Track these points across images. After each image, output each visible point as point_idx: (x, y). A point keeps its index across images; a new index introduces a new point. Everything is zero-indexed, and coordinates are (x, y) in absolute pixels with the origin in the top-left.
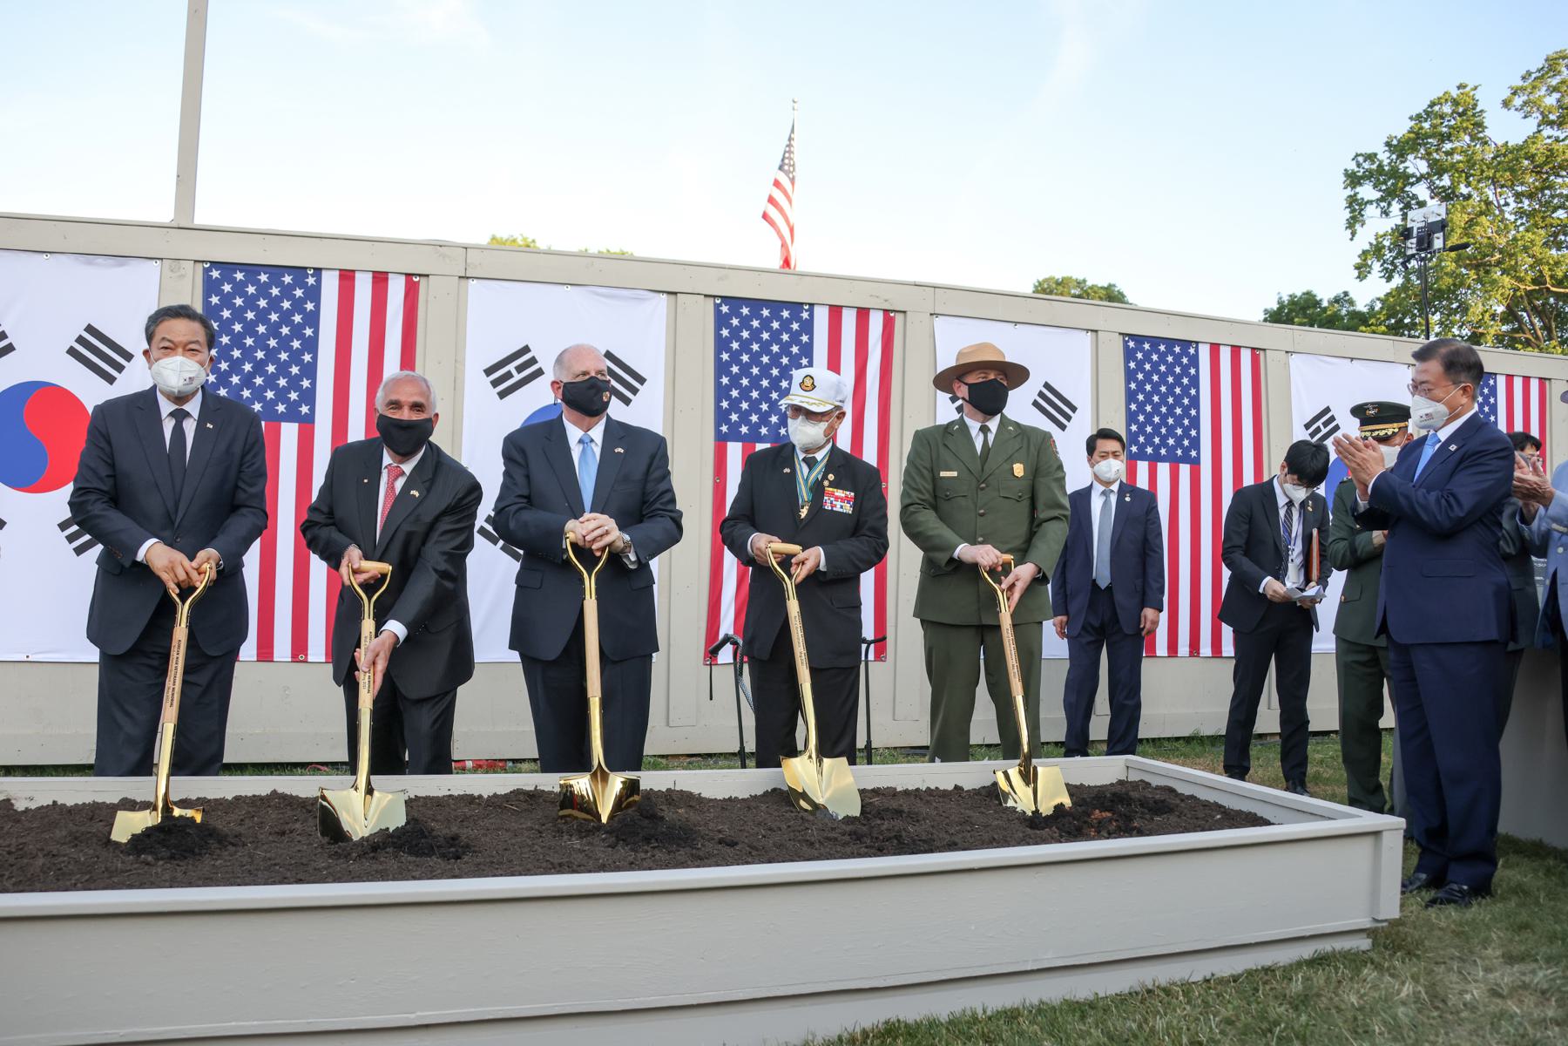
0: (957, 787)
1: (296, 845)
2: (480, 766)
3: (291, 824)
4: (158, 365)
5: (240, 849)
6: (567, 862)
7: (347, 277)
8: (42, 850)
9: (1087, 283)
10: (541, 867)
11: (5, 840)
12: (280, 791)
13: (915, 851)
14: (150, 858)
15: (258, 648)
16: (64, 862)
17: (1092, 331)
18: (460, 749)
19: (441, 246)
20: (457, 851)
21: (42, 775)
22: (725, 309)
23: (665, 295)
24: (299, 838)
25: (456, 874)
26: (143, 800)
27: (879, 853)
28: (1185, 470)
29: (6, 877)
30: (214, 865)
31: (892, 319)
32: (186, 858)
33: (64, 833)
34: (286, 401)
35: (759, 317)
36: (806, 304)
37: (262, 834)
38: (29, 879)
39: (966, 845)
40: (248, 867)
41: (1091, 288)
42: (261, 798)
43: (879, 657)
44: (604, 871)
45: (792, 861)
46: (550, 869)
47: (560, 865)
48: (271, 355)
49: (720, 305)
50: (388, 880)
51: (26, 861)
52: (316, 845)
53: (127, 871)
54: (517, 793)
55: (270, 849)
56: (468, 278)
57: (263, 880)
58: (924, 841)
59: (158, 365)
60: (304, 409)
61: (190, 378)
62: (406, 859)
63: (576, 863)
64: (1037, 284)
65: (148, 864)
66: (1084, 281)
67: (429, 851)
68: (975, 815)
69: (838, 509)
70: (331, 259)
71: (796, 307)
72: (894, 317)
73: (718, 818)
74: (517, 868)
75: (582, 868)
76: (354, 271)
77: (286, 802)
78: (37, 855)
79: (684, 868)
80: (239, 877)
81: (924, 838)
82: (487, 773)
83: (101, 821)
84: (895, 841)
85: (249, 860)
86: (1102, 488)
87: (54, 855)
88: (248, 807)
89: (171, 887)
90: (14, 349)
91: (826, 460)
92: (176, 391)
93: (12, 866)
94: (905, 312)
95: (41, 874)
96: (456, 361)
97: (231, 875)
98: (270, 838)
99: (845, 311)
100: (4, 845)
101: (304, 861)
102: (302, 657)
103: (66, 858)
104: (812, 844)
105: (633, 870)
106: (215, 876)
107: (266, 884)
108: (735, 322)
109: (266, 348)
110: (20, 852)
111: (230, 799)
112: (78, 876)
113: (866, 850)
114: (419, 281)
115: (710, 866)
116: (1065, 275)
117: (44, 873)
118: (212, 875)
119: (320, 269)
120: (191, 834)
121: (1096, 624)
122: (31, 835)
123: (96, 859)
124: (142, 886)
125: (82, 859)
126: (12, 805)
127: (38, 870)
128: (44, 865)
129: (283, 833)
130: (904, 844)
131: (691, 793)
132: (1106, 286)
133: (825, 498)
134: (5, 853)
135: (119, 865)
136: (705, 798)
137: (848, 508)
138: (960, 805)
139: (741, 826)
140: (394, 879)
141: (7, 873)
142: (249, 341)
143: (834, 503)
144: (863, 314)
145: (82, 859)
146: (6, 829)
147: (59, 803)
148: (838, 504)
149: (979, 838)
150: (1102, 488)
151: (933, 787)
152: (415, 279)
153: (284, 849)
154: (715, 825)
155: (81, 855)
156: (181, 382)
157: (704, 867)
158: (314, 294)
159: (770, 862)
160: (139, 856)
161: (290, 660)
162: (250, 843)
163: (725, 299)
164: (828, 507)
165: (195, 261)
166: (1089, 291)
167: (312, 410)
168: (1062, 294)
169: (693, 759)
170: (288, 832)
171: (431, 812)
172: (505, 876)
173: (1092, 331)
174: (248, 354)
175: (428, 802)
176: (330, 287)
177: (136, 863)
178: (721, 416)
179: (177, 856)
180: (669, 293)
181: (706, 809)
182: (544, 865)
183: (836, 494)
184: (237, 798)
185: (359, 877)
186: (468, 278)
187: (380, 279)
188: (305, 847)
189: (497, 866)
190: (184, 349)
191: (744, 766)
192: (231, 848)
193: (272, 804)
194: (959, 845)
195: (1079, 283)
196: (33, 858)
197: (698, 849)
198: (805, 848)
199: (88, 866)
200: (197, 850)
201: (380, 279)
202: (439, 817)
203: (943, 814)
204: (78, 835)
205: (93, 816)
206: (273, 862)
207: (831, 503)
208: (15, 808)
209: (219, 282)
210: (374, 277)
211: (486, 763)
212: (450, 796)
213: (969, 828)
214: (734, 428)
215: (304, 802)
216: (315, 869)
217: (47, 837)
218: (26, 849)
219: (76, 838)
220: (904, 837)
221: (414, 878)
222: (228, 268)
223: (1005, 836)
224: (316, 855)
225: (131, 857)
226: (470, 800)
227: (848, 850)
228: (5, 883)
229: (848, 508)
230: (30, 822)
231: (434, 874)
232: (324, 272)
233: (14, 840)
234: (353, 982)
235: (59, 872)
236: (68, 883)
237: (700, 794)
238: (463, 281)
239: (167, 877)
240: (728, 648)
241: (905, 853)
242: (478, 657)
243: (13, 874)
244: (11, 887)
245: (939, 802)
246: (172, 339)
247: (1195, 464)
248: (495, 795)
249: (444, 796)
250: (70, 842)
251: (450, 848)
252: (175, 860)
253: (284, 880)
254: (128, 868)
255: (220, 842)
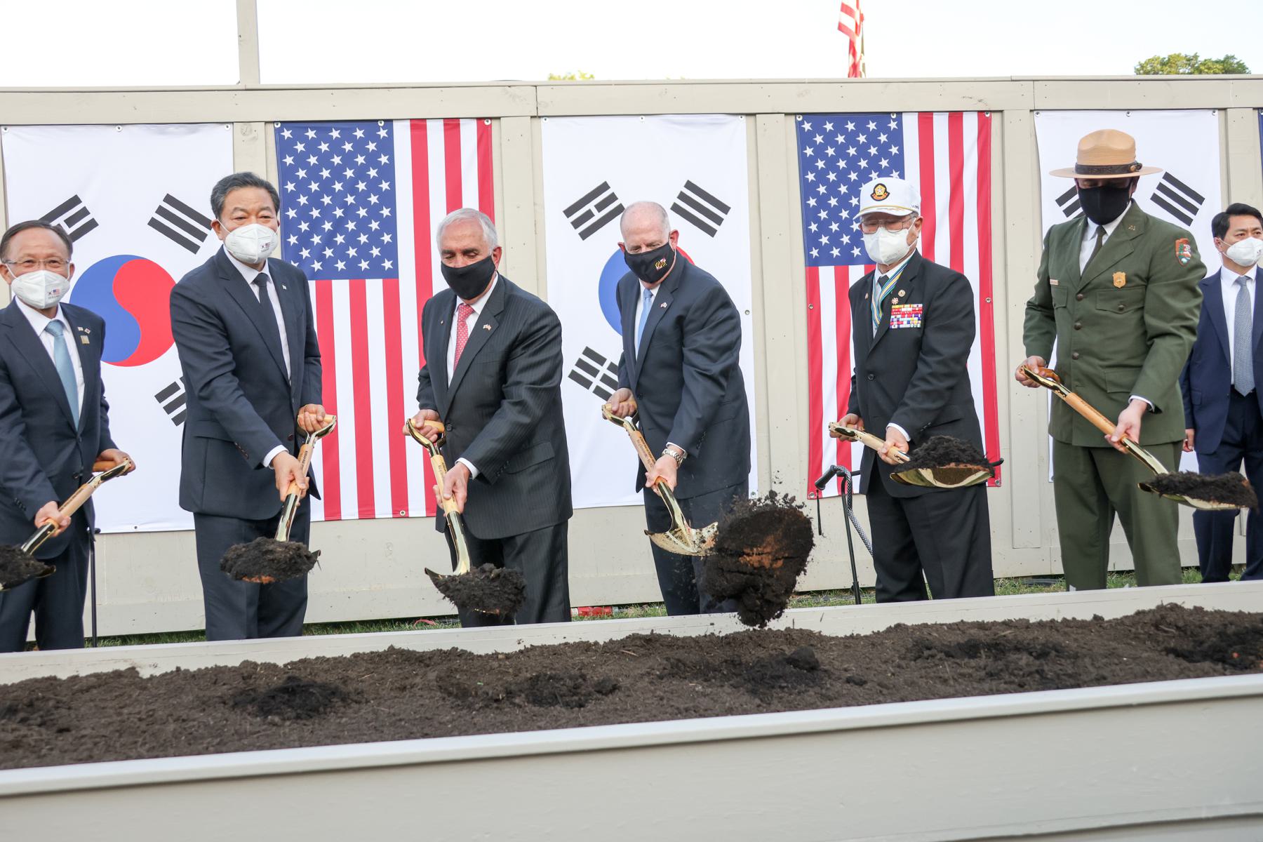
0: (1096, 618)
1: (418, 700)
2: (586, 613)
3: (411, 679)
4: (234, 235)
5: (363, 706)
6: (694, 707)
7: (418, 126)
8: (171, 715)
9: (1199, 59)
10: (666, 713)
11: (135, 707)
12: (397, 646)
13: (1060, 686)
14: (277, 719)
15: (359, 507)
16: (194, 726)
17: (1219, 109)
18: (579, 595)
19: (509, 87)
20: (580, 699)
21: (157, 642)
22: (807, 126)
23: (744, 117)
24: (421, 693)
25: (583, 722)
26: (268, 662)
27: (1021, 689)
28: (374, 288)
29: (139, 744)
30: (340, 723)
31: (989, 120)
32: (311, 717)
33: (191, 698)
34: (368, 257)
35: (866, 131)
36: (893, 113)
37: (383, 690)
38: (162, 745)
39: (1117, 679)
40: (373, 723)
41: (1203, 64)
42: (379, 655)
43: (994, 483)
44: (732, 715)
45: (927, 699)
46: (676, 714)
47: (687, 710)
48: (350, 212)
49: (802, 123)
50: (514, 731)
51: (157, 727)
52: (438, 698)
53: (255, 733)
54: (634, 639)
55: (393, 705)
56: (540, 117)
57: (390, 737)
58: (1070, 676)
59: (234, 235)
60: (387, 265)
61: (266, 244)
62: (530, 709)
63: (702, 707)
64: (1138, 67)
65: (275, 725)
66: (1196, 57)
67: (553, 700)
68: (1121, 648)
69: (905, 325)
70: (401, 109)
71: (882, 117)
72: (491, 125)
73: (842, 655)
74: (642, 714)
75: (709, 712)
76: (425, 120)
77: (404, 657)
78: (168, 720)
79: (813, 709)
80: (366, 734)
81: (1070, 672)
82: (594, 619)
83: (224, 684)
84: (1037, 676)
85: (374, 717)
86: (1236, 276)
87: (184, 720)
88: (367, 663)
89: (301, 746)
90: (97, 225)
91: (897, 277)
92: (256, 258)
93: (144, 732)
94: (1001, 111)
95: (174, 739)
96: (535, 204)
97: (358, 733)
98: (392, 694)
99: (936, 117)
100: (134, 712)
101: (428, 715)
102: (403, 513)
103: (195, 723)
104: (945, 681)
105: (761, 712)
106: (342, 734)
107: (393, 739)
108: (819, 139)
109: (344, 205)
110: (151, 719)
111: (348, 656)
112: (209, 740)
113: (1006, 686)
114: (491, 124)
115: (840, 706)
116: (1172, 53)
117: (176, 738)
118: (339, 734)
119: (391, 121)
120: (314, 694)
121: (1237, 437)
122: (159, 700)
123: (225, 722)
124: (271, 747)
125: (212, 723)
126: (138, 673)
127: (170, 736)
128: (175, 730)
129: (404, 688)
130: (1048, 679)
131: (811, 632)
132: (1222, 59)
133: (892, 317)
134: (136, 720)
135: (248, 727)
136: (825, 636)
137: (916, 322)
138: (1101, 636)
139: (868, 664)
140: (520, 730)
141: (140, 740)
142: (327, 200)
143: (901, 320)
144: (956, 118)
145: (212, 723)
146: (134, 696)
147: (182, 669)
148: (905, 320)
149: (1130, 671)
150: (1236, 276)
151: (1069, 618)
152: (486, 123)
153: (407, 704)
154: (840, 664)
155: (210, 718)
156: (261, 249)
157: (834, 707)
158: (387, 146)
159: (903, 700)
160: (266, 717)
161: (391, 516)
162: (373, 699)
163: (807, 116)
164: (894, 326)
165: (266, 122)
166: (1202, 68)
167: (395, 264)
168: (1169, 73)
169: (803, 597)
170: (409, 687)
171: (549, 661)
172: (632, 722)
173: (1219, 109)
174: (326, 212)
175: (545, 650)
176: (402, 137)
177: (264, 725)
178: (810, 240)
179: (303, 716)
180: (747, 115)
181: (828, 648)
182: (669, 710)
183: (903, 310)
184: (356, 656)
185: (484, 729)
186: (540, 117)
187: (452, 125)
188: (427, 701)
189: (621, 713)
190: (257, 215)
191: (858, 602)
192: (353, 705)
193: (390, 659)
194: (1109, 680)
195: (1189, 60)
196: (164, 723)
197: (828, 689)
198: (939, 686)
199: (217, 730)
200: (321, 709)
201: (452, 125)
202: (557, 666)
203: (1085, 646)
204: (205, 699)
205: (217, 680)
206: (398, 718)
207: (898, 321)
208: (140, 675)
209: (292, 142)
210: (445, 125)
211: (592, 610)
212: (566, 644)
213: (1116, 661)
214: (825, 251)
215: (422, 656)
216: (440, 723)
217: (175, 702)
218: (156, 715)
219: (204, 703)
220: (1046, 671)
221: (540, 728)
222: (298, 126)
223: (1159, 670)
224: (438, 708)
225: (258, 719)
226: (585, 647)
227: (986, 686)
228: (139, 749)
229: (916, 322)
230: (156, 689)
231: (559, 723)
232: (395, 123)
233: (144, 706)
234: (487, 836)
235: (190, 737)
236: (200, 747)
237: (820, 632)
238: (535, 121)
239: (295, 737)
240: (834, 481)
241: (1050, 688)
242: (575, 505)
243: (147, 741)
244: (145, 753)
245: (1077, 634)
246: (245, 208)
247: (391, 279)
248: (611, 641)
249: (560, 645)
250: (198, 706)
251: (572, 696)
252: (302, 719)
253: (410, 736)
254: (257, 730)
255: (343, 700)
